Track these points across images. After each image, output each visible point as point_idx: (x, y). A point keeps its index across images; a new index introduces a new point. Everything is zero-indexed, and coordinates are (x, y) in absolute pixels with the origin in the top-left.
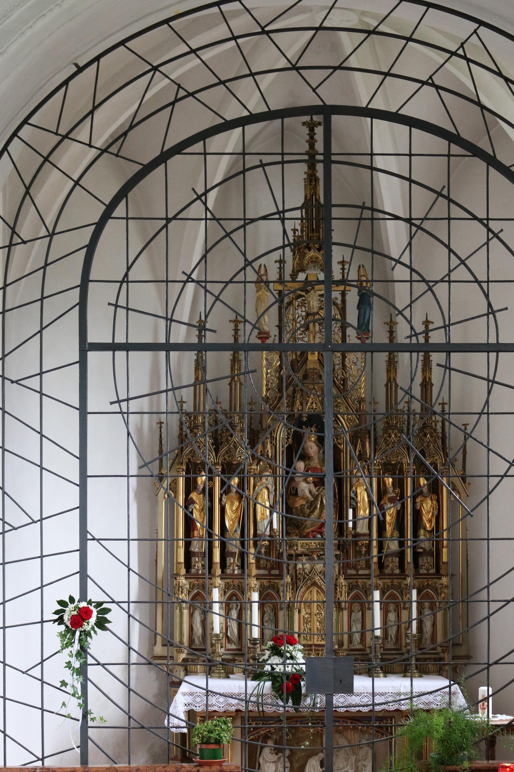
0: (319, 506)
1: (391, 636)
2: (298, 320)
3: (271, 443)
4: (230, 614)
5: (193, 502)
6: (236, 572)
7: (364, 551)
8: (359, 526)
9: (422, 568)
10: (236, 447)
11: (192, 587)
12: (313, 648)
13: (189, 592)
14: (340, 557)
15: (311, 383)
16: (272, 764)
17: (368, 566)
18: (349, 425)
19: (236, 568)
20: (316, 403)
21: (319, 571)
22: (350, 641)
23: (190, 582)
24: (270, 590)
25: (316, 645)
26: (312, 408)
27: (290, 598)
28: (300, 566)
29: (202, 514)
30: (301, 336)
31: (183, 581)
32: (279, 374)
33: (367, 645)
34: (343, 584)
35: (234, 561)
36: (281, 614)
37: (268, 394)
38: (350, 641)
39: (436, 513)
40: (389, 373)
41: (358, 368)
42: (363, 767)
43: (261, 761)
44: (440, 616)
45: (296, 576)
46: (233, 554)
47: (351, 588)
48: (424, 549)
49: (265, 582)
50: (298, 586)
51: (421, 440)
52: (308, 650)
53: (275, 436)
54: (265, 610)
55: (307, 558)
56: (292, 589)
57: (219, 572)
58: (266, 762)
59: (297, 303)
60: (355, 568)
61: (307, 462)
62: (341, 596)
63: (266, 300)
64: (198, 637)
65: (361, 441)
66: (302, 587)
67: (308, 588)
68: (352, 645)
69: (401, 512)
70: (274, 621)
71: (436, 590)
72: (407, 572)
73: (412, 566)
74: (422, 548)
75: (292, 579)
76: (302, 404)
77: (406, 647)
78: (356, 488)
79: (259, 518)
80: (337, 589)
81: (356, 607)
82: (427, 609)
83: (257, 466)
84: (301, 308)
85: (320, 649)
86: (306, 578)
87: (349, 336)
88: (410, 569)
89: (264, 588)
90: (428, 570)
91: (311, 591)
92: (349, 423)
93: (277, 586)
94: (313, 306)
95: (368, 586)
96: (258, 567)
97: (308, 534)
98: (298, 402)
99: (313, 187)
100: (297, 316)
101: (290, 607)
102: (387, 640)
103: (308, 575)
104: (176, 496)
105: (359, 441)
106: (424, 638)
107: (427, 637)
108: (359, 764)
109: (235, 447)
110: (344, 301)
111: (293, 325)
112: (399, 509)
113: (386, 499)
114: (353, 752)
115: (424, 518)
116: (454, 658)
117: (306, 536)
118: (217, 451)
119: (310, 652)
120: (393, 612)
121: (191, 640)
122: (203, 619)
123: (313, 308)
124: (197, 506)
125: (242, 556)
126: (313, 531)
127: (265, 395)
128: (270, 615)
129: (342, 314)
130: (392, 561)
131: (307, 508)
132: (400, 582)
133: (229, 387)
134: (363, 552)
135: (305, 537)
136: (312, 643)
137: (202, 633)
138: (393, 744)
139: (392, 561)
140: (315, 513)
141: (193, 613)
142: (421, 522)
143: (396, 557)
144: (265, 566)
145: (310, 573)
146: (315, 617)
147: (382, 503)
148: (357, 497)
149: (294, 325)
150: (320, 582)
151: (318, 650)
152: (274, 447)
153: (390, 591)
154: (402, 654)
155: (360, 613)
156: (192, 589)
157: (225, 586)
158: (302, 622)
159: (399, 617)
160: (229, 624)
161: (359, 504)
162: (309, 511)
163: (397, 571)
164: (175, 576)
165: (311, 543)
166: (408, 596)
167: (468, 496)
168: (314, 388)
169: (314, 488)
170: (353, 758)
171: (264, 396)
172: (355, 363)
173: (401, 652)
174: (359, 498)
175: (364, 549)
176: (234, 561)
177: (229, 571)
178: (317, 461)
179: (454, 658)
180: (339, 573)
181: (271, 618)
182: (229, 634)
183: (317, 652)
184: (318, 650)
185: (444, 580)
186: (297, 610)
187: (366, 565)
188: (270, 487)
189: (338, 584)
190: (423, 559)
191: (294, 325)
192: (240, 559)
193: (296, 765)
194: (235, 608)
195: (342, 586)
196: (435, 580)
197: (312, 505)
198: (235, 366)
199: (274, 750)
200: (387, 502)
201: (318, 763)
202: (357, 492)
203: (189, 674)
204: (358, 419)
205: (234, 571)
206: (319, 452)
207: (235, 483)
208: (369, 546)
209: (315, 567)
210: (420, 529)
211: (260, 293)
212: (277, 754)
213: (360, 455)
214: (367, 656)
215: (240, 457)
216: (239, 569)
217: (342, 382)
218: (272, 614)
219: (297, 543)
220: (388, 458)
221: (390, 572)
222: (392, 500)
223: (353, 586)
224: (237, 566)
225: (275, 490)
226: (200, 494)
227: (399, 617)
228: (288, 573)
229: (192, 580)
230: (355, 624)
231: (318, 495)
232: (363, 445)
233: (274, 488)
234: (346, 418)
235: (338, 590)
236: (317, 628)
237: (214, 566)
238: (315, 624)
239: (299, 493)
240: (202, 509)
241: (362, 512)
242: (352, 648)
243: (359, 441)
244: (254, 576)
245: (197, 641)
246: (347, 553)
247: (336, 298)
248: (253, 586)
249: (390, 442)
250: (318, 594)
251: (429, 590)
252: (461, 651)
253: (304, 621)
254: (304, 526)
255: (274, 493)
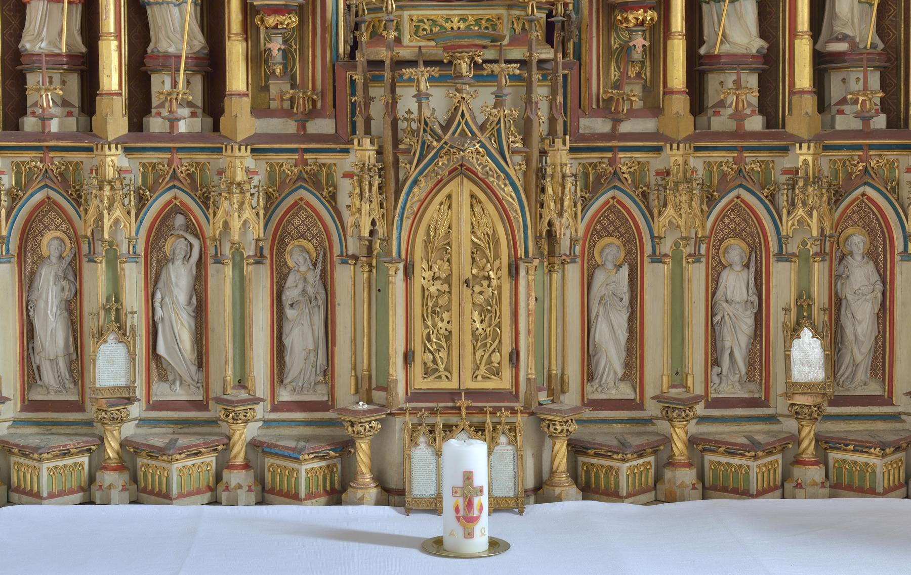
1: (731, 354)
6: (182, 127)
7: (639, 49)
9: (841, 112)
12: (463, 403)
14: (556, 70)
19: (185, 112)
22: (589, 374)
23: (17, 165)
24: (302, 193)
25: (472, 394)
27: (373, 223)
28: (407, 102)
34: (568, 170)
35: (175, 84)
45: (396, 141)
46: (169, 63)
50: (401, 176)
52: (445, 411)
54: (290, 263)
55: (435, 71)
62: (560, 214)
64: (54, 361)
66: (415, 182)
67: (440, 184)
68: (596, 384)
70: (321, 302)
74: (844, 38)
75: (380, 152)
77: (787, 395)
80: (543, 190)
82: (858, 258)
85: (488, 405)
90: (866, 120)
91: (449, 197)
93: (329, 175)
95: (653, 179)
96: (259, 111)
102: (716, 370)
103: (439, 139)
106: (847, 360)
107: (859, 358)
119: (453, 419)
120: (738, 268)
122: (67, 294)
128: (305, 280)
130: (738, 84)
132: (766, 163)
134: (637, 55)
136: (453, 385)
139: (738, 84)
141: (33, 274)
143: (752, 70)
145: (445, 128)
146: (467, 292)
150: (480, 162)
151: (482, 411)
154: (772, 419)
155: (625, 271)
157: (144, 176)
160: (159, 313)
163: (755, 123)
165: (448, 20)
175: (639, 41)
176: (175, 84)
177: (155, 124)
180: (552, 132)
181: (310, 290)
182: (161, 349)
183: (477, 419)
184: (482, 411)
186: (401, 266)
189: (549, 171)
190: (844, 80)
194: (180, 256)
196: (891, 155)
203: (15, 496)
205: (173, 121)
209: (463, 107)
216: (193, 115)
218: (313, 277)
219: (400, 17)
221: (731, 126)
223: (599, 177)
224: (190, 104)
227: (760, 286)
228: (368, 131)
229: (26, 156)
230: (606, 312)
235: (550, 191)
236: (474, 332)
237: (102, 104)
238: (468, 322)
244: (246, 142)
246: (578, 56)
248: (239, 178)
250: (477, 208)
251: (870, 192)
253: (424, 304)
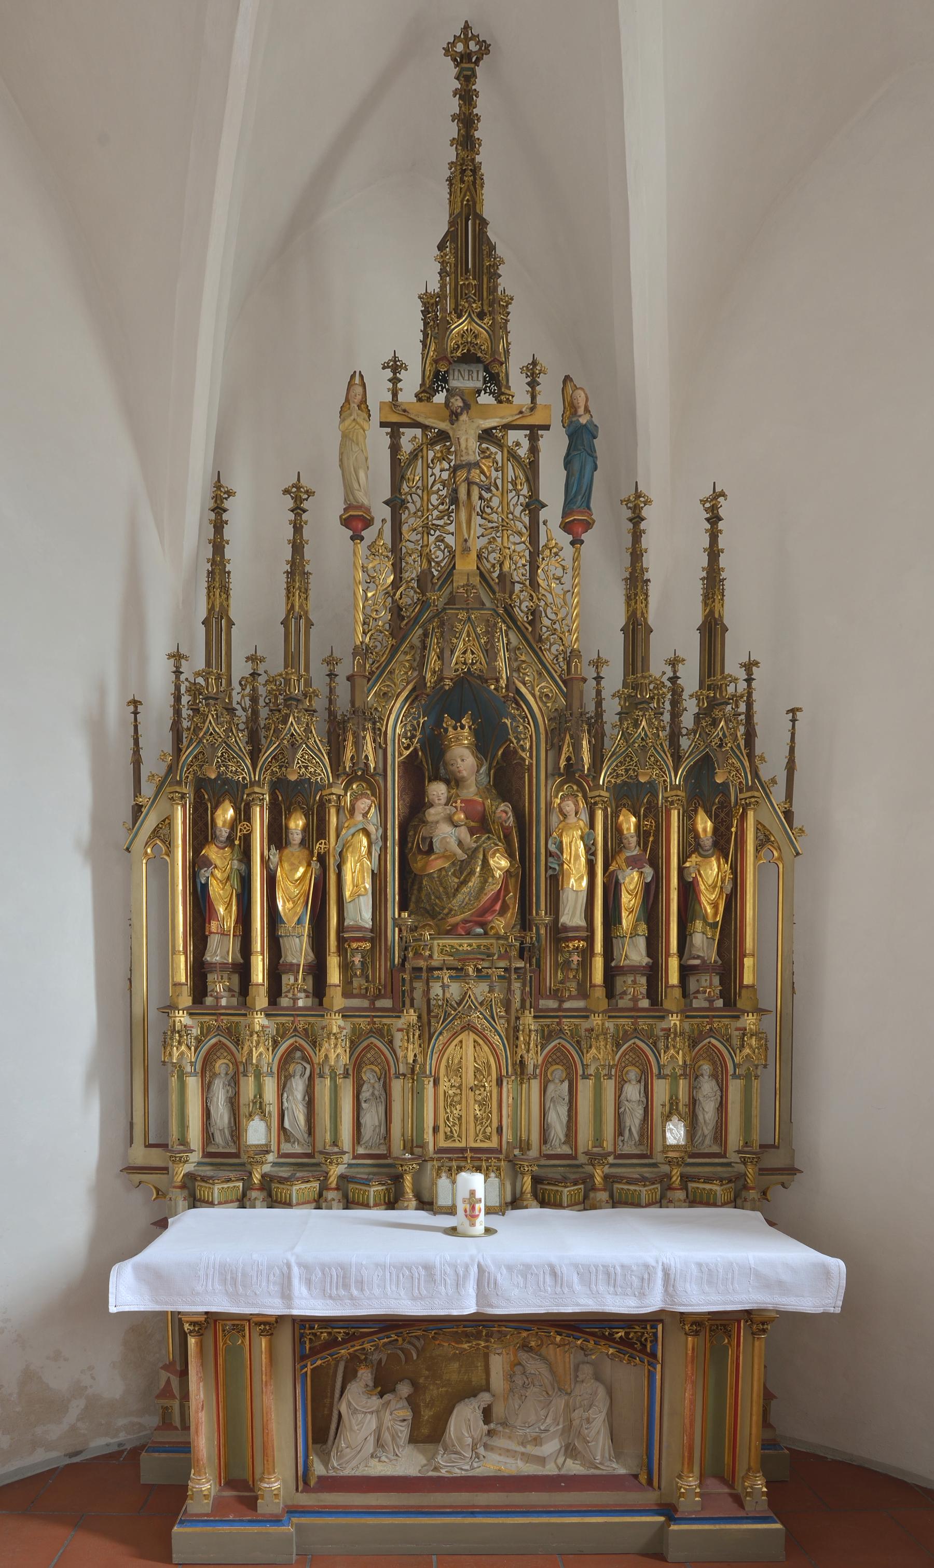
0: (478, 869)
1: (630, 1130)
2: (435, 488)
3: (374, 741)
4: (288, 1085)
5: (207, 863)
6: (300, 1003)
7: (576, 963)
8: (566, 911)
9: (696, 998)
10: (294, 746)
11: (206, 1032)
12: (469, 1154)
13: (199, 1041)
14: (525, 973)
15: (463, 609)
16: (369, 1416)
17: (584, 992)
18: (544, 708)
20: (473, 653)
21: (480, 999)
22: (544, 1138)
23: (201, 1023)
24: (373, 1040)
25: (473, 1150)
26: (465, 663)
27: (415, 1056)
29: (228, 887)
30: (441, 522)
31: (182, 1018)
32: (394, 601)
33: (581, 1149)
34: (532, 1027)
36: (397, 1086)
37: (367, 640)
38: (544, 1138)
39: (728, 887)
40: (633, 602)
41: (566, 589)
42: (584, 1423)
43: (343, 1408)
44: (735, 1088)
45: (429, 1011)
47: (547, 1036)
48: (704, 961)
49: (363, 1023)
51: (704, 735)
53: (383, 729)
55: (453, 973)
56: (419, 1036)
57: (261, 1000)
58: (355, 1412)
59: (431, 454)
60: (555, 994)
61: (453, 791)
62: (528, 1051)
63: (361, 439)
64: (222, 1131)
65: (572, 737)
66: (441, 1033)
67: (456, 1035)
68: (548, 1146)
69: (653, 887)
71: (727, 1040)
72: (668, 1004)
73: (677, 993)
74: (698, 957)
75: (419, 1017)
76: (440, 657)
78: (561, 836)
79: (347, 894)
80: (517, 1038)
81: (558, 1071)
82: (706, 1077)
83: (346, 789)
84: (441, 463)
85: (484, 1156)
86: (450, 1014)
87: (545, 523)
88: (672, 1000)
89: (361, 1034)
91: (461, 1042)
92: (545, 703)
93: (389, 1030)
94: (466, 448)
96: (346, 994)
97: (455, 926)
98: (433, 656)
99: (468, 189)
100: (431, 480)
101: (414, 1073)
103: (455, 1010)
104: (170, 852)
105: (568, 737)
106: (700, 1133)
107: (706, 1132)
108: (575, 1415)
109: (293, 745)
110: (534, 450)
111: (422, 499)
112: (649, 880)
113: (621, 859)
114: (560, 1389)
115: (703, 899)
116: (763, 1171)
117: (451, 932)
118: (254, 756)
119: (462, 1164)
120: (634, 1082)
121: (208, 1136)
123: (468, 454)
124: (218, 873)
125: (318, 971)
126: (465, 921)
127: (362, 643)
129: (530, 477)
130: (634, 982)
131: (454, 874)
133: (282, 629)
134: (574, 966)
135: (448, 932)
136: (463, 1145)
137: (230, 1122)
138: (658, 1377)
139: (634, 982)
140: (470, 884)
141: (210, 1083)
142: (697, 907)
143: (643, 975)
144: (363, 991)
145: (459, 1004)
147: (611, 868)
148: (562, 853)
149: (425, 498)
151: (480, 1159)
152: (380, 752)
153: (630, 1042)
155: (566, 1084)
156: (206, 1036)
157: (277, 1030)
158: (441, 1104)
159: (647, 1093)
160: (286, 1104)
161: (565, 866)
162: (456, 880)
163: (645, 1003)
164: (169, 1008)
166: (672, 1051)
167: (798, 854)
168: (469, 619)
169: (469, 836)
170: (560, 1403)
171: (358, 643)
172: (559, 579)
173: (651, 1161)
174: (566, 856)
175: (575, 958)
176: (296, 980)
177: (285, 1002)
178: (473, 789)
179: (763, 1171)
180: (523, 1006)
181: (376, 1093)
182: (287, 1124)
183: (477, 1163)
184: (480, 1159)
185: (749, 1021)
186: (432, 1079)
187: (578, 990)
188: (372, 829)
189: (521, 1028)
191: (425, 498)
192: (310, 980)
193: (427, 1414)
195: (530, 1031)
197: (463, 869)
198: (294, 581)
199: (375, 1386)
200: (624, 867)
201: (479, 1414)
202: (561, 842)
203: (198, 1204)
204: (565, 696)
205: (295, 1000)
206: (478, 771)
207: (297, 825)
208: (587, 953)
209: (470, 992)
210: (693, 920)
211: (347, 422)
212: (381, 1395)
213: (568, 766)
214: (581, 1170)
215: (306, 767)
216: (307, 997)
217: (530, 618)
218: (379, 1086)
220: (631, 772)
222: (633, 863)
223: (550, 1032)
225: (385, 838)
226: (223, 848)
227: (647, 1093)
229: (206, 1019)
231: (476, 850)
232: (577, 747)
233: (380, 831)
234: (537, 694)
235: (522, 1039)
236: (475, 1116)
237: (252, 990)
239: (437, 845)
240: (228, 879)
241: (572, 880)
242: (549, 1152)
243: (568, 737)
244: (339, 1011)
245: (219, 1139)
246: (538, 966)
247: (518, 444)
249: (637, 738)
251: (713, 1041)
252: (774, 1160)
254: (446, 911)
255: (380, 844)
